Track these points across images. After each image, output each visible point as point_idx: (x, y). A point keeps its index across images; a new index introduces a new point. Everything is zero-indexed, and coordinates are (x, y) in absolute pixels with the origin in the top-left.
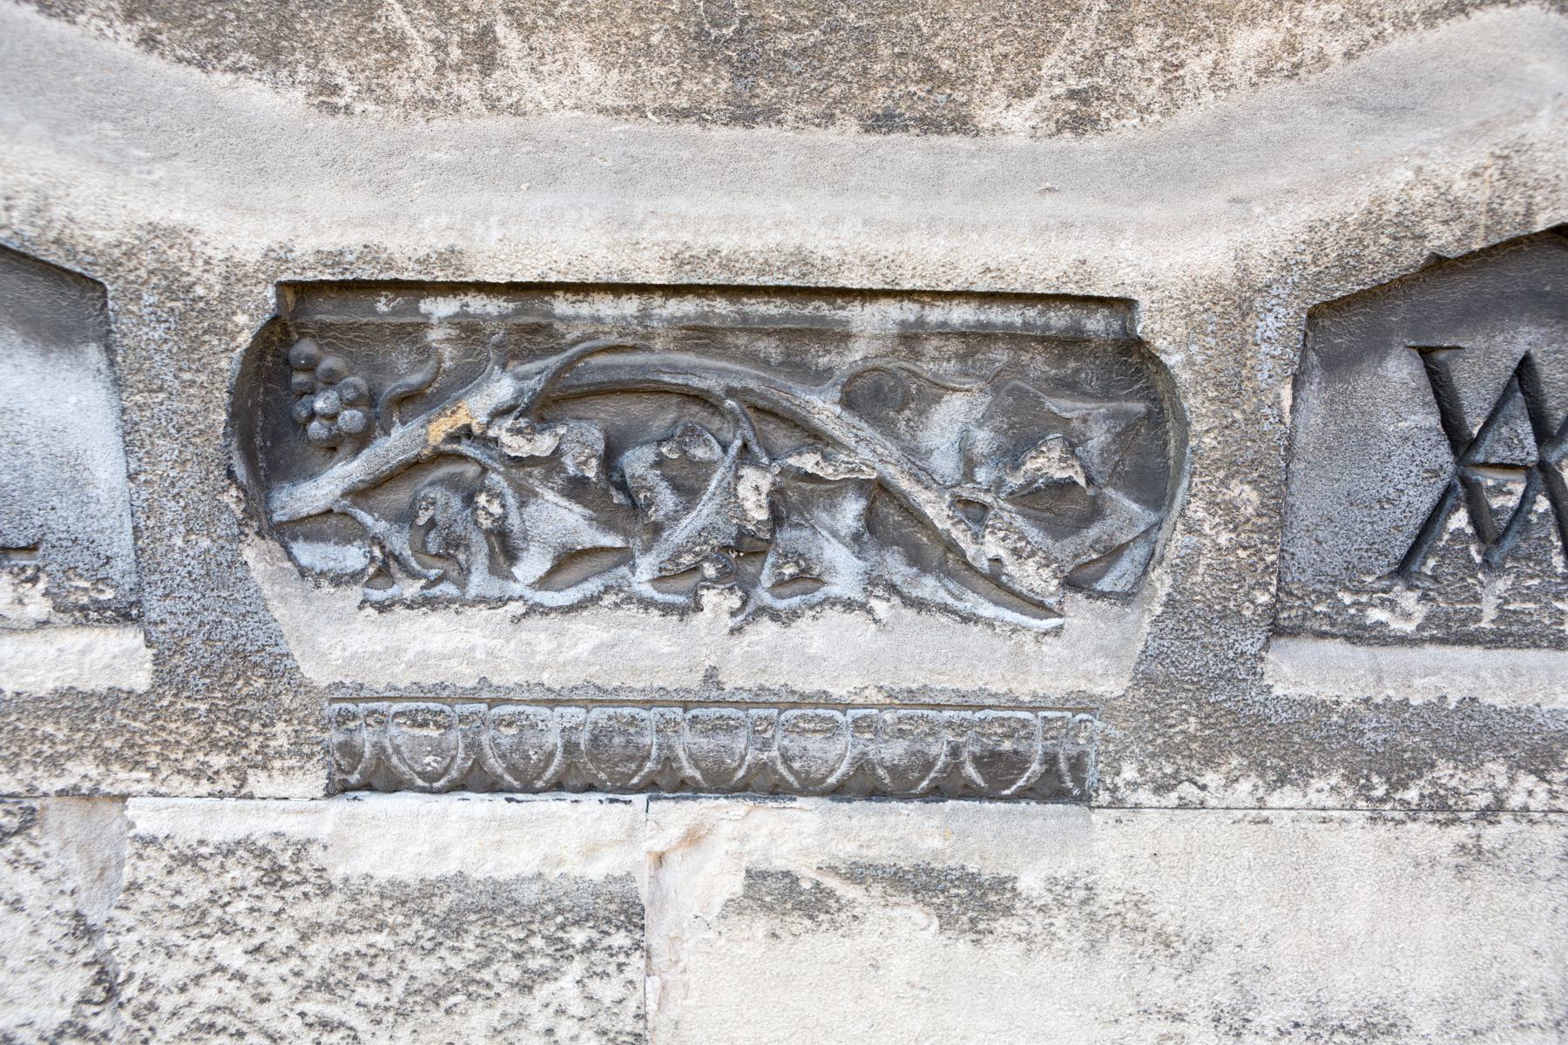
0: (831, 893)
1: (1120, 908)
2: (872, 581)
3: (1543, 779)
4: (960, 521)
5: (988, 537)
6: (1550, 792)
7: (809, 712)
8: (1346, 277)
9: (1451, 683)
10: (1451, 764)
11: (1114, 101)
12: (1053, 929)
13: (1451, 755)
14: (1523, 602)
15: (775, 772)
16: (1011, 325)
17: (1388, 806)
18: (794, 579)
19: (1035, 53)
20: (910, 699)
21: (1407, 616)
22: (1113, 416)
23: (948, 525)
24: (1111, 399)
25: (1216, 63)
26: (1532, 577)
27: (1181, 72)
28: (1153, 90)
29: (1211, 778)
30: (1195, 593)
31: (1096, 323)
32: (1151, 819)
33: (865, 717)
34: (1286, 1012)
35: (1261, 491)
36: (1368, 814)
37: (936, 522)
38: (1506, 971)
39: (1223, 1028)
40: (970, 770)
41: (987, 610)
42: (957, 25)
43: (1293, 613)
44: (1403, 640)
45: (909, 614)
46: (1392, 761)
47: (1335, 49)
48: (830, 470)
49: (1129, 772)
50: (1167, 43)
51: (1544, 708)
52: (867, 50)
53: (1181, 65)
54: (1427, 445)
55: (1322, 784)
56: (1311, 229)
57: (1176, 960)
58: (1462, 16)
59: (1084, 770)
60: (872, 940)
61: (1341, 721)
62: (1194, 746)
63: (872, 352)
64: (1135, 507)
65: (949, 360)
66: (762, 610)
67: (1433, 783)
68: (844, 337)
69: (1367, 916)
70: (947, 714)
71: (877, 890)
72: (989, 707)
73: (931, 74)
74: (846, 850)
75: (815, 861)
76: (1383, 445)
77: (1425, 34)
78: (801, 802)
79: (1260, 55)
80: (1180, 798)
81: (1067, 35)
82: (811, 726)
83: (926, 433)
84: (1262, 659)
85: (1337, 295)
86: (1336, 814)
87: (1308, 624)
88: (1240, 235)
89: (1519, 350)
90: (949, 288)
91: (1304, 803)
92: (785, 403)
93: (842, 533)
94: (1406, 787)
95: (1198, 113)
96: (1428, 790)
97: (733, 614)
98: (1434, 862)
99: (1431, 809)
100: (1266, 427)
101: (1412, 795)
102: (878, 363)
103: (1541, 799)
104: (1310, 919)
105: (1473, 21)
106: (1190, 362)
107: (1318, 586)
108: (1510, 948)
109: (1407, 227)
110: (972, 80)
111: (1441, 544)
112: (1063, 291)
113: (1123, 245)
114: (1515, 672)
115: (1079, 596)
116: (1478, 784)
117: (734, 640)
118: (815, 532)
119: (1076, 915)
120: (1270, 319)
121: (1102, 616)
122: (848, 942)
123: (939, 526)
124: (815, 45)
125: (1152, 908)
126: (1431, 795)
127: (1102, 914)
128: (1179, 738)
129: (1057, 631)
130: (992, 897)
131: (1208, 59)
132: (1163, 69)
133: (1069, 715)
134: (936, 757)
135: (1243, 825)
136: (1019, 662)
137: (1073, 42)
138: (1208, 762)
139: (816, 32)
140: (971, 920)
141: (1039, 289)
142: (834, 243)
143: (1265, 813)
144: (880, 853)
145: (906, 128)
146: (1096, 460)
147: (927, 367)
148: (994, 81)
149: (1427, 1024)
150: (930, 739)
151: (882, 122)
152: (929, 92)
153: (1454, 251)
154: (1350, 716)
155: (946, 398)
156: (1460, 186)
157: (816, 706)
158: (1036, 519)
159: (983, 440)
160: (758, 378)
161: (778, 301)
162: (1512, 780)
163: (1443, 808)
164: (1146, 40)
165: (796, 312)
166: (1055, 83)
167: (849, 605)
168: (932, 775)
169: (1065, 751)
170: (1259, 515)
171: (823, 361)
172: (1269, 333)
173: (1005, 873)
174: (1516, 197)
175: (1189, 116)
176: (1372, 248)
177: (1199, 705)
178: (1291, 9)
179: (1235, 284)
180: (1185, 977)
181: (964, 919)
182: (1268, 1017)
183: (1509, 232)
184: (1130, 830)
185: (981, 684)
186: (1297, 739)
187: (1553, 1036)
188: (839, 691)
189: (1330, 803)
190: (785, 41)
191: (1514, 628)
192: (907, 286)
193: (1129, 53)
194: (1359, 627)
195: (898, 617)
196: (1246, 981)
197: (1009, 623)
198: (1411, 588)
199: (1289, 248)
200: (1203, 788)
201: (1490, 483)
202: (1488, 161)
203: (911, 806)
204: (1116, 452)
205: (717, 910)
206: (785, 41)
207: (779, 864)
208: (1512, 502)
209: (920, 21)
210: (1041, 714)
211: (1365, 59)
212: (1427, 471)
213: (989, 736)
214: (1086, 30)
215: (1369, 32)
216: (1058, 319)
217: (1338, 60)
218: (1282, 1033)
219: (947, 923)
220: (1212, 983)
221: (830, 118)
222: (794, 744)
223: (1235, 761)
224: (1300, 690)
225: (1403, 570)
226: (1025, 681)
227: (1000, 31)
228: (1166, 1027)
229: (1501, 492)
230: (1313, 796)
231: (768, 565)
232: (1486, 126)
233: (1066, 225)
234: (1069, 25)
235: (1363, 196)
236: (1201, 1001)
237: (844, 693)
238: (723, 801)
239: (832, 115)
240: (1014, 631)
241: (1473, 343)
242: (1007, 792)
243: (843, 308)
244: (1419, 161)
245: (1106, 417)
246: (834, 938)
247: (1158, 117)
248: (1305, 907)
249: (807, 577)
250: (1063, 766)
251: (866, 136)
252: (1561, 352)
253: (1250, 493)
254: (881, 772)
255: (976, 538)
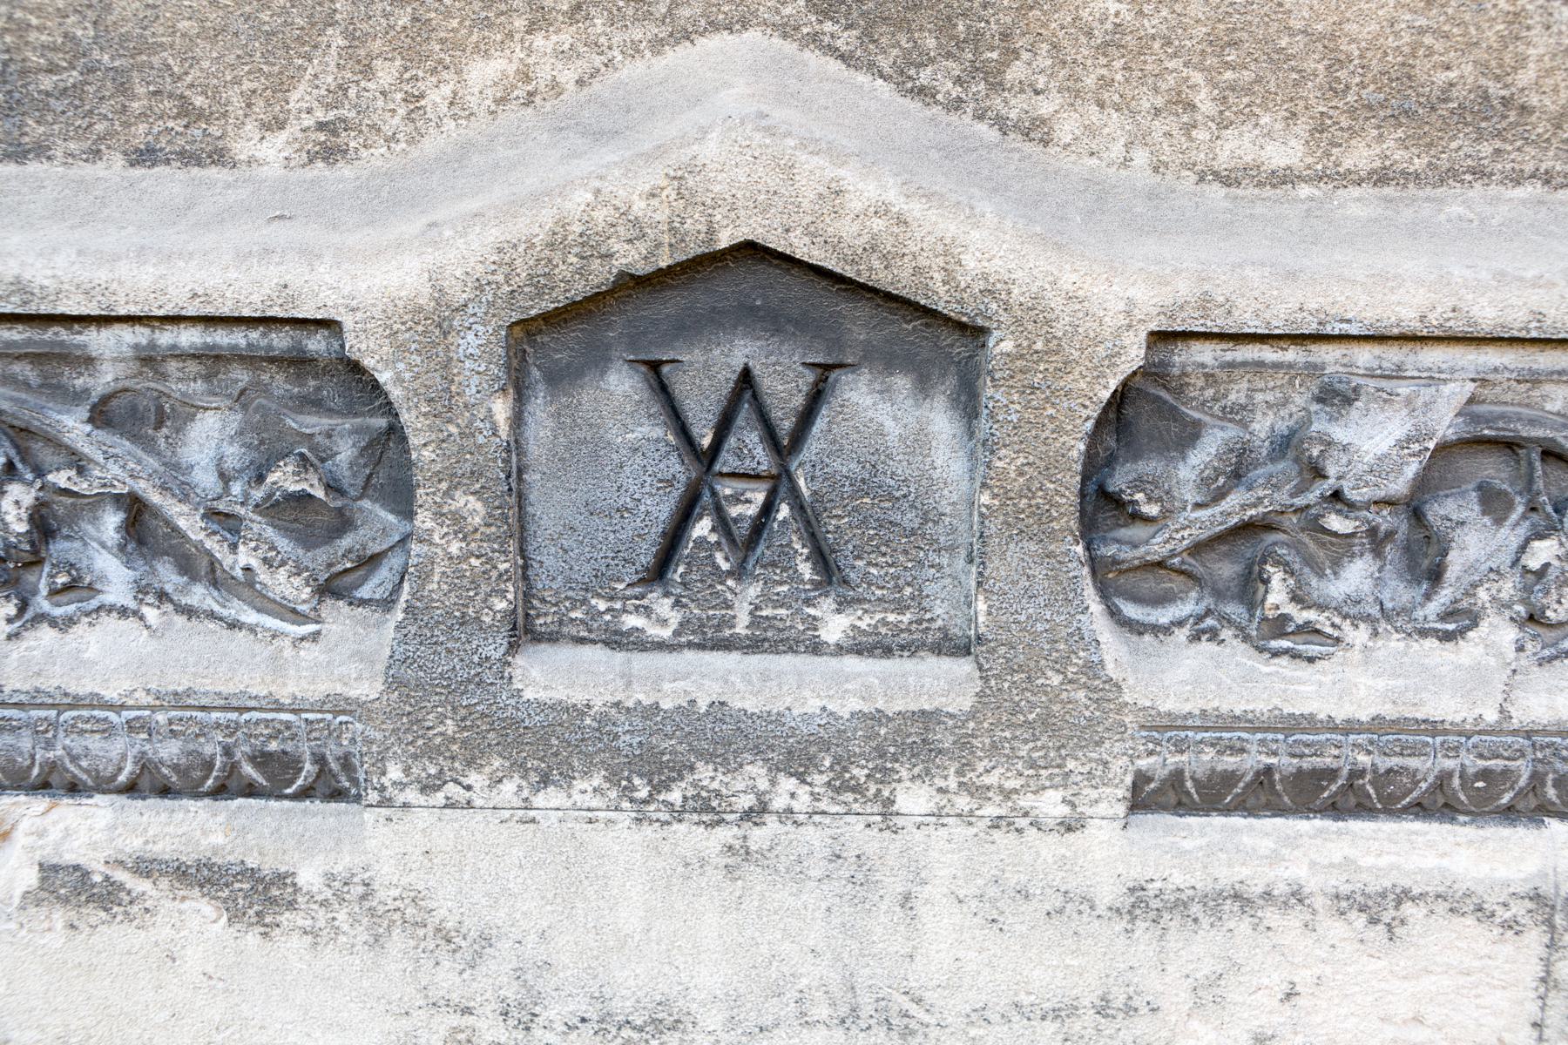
0: (121, 887)
1: (398, 903)
2: (141, 590)
3: (804, 782)
4: (214, 533)
5: (241, 548)
6: (812, 794)
7: (85, 713)
8: (540, 295)
9: (700, 687)
10: (711, 767)
11: (361, 131)
12: (336, 923)
13: (709, 757)
14: (775, 608)
15: (67, 771)
16: (235, 347)
17: (652, 807)
18: (67, 588)
19: (281, 88)
20: (178, 700)
21: (664, 622)
22: (356, 431)
23: (202, 536)
24: (356, 415)
25: (455, 93)
26: (781, 583)
27: (423, 103)
28: (396, 120)
29: (473, 778)
30: (433, 600)
31: (316, 343)
32: (422, 818)
33: (138, 718)
34: (571, 1008)
35: (485, 502)
36: (634, 815)
37: (189, 533)
38: (785, 969)
39: (512, 1022)
40: (248, 769)
41: (250, 617)
42: (206, 64)
43: (549, 619)
44: (661, 646)
45: (180, 620)
46: (654, 763)
47: (568, 77)
48: (85, 485)
49: (394, 772)
50: (407, 76)
51: (795, 712)
52: (124, 89)
53: (422, 96)
54: (657, 455)
55: (585, 785)
56: (500, 250)
57: (458, 955)
58: (688, 44)
59: (355, 771)
60: (166, 932)
61: (595, 725)
62: (455, 747)
63: (121, 374)
64: (391, 518)
65: (195, 380)
66: (41, 618)
67: (695, 785)
68: (88, 361)
69: (642, 914)
70: (215, 715)
71: (164, 883)
72: (254, 709)
73: (186, 110)
74: (133, 844)
75: (102, 857)
76: (614, 456)
77: (653, 61)
78: (98, 799)
79: (496, 84)
80: (447, 798)
81: (310, 70)
82: (88, 726)
83: (185, 449)
84: (509, 664)
85: (533, 312)
86: (601, 814)
87: (565, 630)
88: (432, 257)
89: (738, 362)
90: (161, 313)
91: (569, 804)
92: (36, 423)
93: (109, 544)
94: (668, 789)
95: (441, 140)
96: (691, 792)
97: (10, 621)
98: (703, 862)
99: (695, 810)
100: (481, 440)
101: (675, 796)
102: (127, 384)
103: (803, 802)
104: (586, 916)
105: (698, 47)
106: (399, 380)
107: (570, 593)
108: (786, 946)
109: (592, 247)
110: (225, 115)
111: (686, 552)
112: (269, 314)
113: (321, 270)
114: (765, 677)
115: (341, 603)
116: (740, 786)
117: (12, 645)
118: (85, 544)
119: (357, 909)
120: (470, 337)
121: (364, 623)
122: (143, 934)
123: (193, 537)
124: (74, 86)
125: (431, 904)
126: (693, 797)
127: (381, 909)
128: (438, 740)
129: (315, 637)
130: (275, 892)
131: (446, 90)
132: (405, 100)
133: (329, 716)
134: (213, 757)
135: (512, 824)
136: (277, 665)
137: (316, 76)
138: (470, 763)
139: (75, 73)
140: (258, 914)
141: (246, 313)
142: (49, 273)
143: (532, 813)
144: (164, 849)
145: (168, 162)
146: (347, 473)
147: (176, 387)
148: (246, 116)
149: (713, 1020)
150: (202, 740)
151: (145, 156)
152: (186, 127)
153: (642, 269)
154: (603, 719)
155: (199, 416)
156: (639, 207)
157: (92, 707)
158: (286, 530)
159: (234, 455)
160: (12, 399)
161: (20, 327)
162: (773, 782)
163: (707, 809)
164: (386, 74)
165: (37, 337)
166: (303, 116)
167: (123, 612)
168: (215, 774)
169: (332, 752)
170: (488, 525)
171: (79, 382)
172: (470, 350)
173: (283, 869)
174: (697, 216)
175: (432, 144)
176: (562, 267)
177: (454, 708)
178: (522, 41)
179: (433, 304)
180: (468, 972)
181: (251, 912)
182: (555, 1012)
183: (694, 250)
184: (401, 828)
185: (242, 687)
186: (554, 741)
187: (839, 1034)
188: (111, 694)
189: (594, 803)
190: (47, 82)
191: (770, 634)
192: (122, 312)
193: (370, 85)
194: (616, 632)
195: (170, 623)
196: (529, 977)
197: (269, 629)
198: (667, 594)
199: (480, 268)
200: (469, 788)
201: (728, 492)
202: (665, 183)
203: (200, 804)
204: (365, 466)
205: (17, 901)
206: (47, 82)
207: (69, 858)
208: (752, 510)
209: (171, 61)
210: (304, 716)
211: (596, 85)
212: (660, 481)
213: (256, 737)
214: (327, 65)
215: (598, 60)
216: (280, 340)
217: (571, 87)
218: (570, 1028)
219: (235, 917)
220: (494, 979)
221: (96, 154)
222: (76, 743)
223: (497, 762)
224: (550, 694)
225: (658, 572)
226: (285, 685)
227: (246, 68)
228: (456, 1020)
229: (738, 501)
230: (577, 797)
231: (44, 575)
232: (661, 150)
233: (267, 252)
234: (310, 60)
235: (547, 217)
236: (487, 996)
237: (115, 695)
238: (22, 798)
239: (99, 151)
240: (274, 637)
241: (692, 356)
242: (289, 791)
243: (80, 333)
244: (597, 184)
245: (351, 433)
246: (129, 929)
247: (404, 145)
248: (579, 905)
249: (76, 586)
250: (334, 766)
251: (131, 170)
252: (780, 364)
253: (475, 504)
254: (165, 771)
255: (234, 547)
